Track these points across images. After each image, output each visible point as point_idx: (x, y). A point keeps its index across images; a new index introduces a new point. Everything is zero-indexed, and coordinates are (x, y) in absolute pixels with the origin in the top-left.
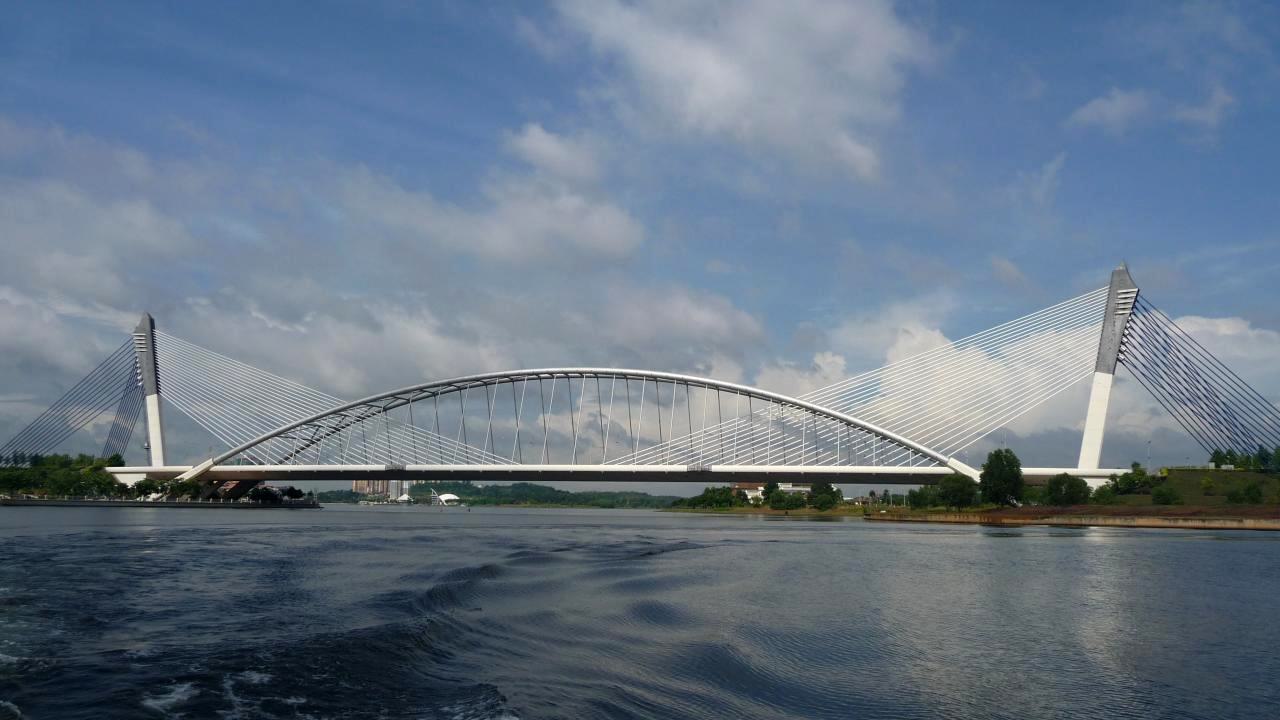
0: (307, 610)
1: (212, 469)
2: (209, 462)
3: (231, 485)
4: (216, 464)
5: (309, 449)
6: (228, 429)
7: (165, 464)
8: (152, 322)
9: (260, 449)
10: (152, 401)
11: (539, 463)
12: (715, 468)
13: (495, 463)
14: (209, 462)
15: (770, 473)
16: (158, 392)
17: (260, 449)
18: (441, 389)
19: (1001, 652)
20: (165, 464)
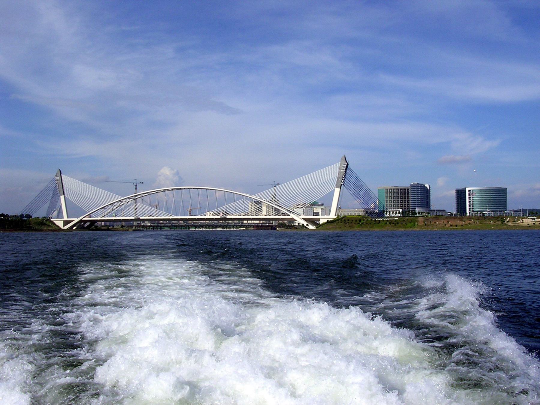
0: (197, 266)
1: (83, 219)
2: (82, 217)
3: (88, 224)
4: (84, 217)
5: (113, 211)
6: (497, 197)
7: (68, 218)
8: (60, 171)
9: (95, 214)
10: (62, 197)
11: (187, 216)
12: (141, 218)
13: (129, 216)
14: (82, 217)
15: (115, 220)
16: (64, 195)
17: (95, 214)
18: (158, 192)
19: (358, 273)
20: (68, 218)
